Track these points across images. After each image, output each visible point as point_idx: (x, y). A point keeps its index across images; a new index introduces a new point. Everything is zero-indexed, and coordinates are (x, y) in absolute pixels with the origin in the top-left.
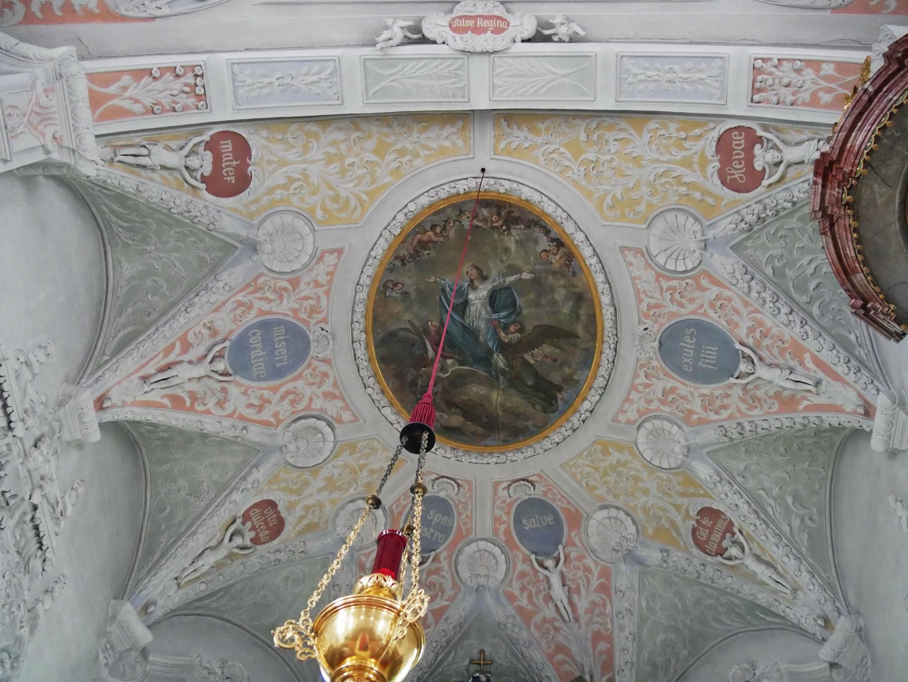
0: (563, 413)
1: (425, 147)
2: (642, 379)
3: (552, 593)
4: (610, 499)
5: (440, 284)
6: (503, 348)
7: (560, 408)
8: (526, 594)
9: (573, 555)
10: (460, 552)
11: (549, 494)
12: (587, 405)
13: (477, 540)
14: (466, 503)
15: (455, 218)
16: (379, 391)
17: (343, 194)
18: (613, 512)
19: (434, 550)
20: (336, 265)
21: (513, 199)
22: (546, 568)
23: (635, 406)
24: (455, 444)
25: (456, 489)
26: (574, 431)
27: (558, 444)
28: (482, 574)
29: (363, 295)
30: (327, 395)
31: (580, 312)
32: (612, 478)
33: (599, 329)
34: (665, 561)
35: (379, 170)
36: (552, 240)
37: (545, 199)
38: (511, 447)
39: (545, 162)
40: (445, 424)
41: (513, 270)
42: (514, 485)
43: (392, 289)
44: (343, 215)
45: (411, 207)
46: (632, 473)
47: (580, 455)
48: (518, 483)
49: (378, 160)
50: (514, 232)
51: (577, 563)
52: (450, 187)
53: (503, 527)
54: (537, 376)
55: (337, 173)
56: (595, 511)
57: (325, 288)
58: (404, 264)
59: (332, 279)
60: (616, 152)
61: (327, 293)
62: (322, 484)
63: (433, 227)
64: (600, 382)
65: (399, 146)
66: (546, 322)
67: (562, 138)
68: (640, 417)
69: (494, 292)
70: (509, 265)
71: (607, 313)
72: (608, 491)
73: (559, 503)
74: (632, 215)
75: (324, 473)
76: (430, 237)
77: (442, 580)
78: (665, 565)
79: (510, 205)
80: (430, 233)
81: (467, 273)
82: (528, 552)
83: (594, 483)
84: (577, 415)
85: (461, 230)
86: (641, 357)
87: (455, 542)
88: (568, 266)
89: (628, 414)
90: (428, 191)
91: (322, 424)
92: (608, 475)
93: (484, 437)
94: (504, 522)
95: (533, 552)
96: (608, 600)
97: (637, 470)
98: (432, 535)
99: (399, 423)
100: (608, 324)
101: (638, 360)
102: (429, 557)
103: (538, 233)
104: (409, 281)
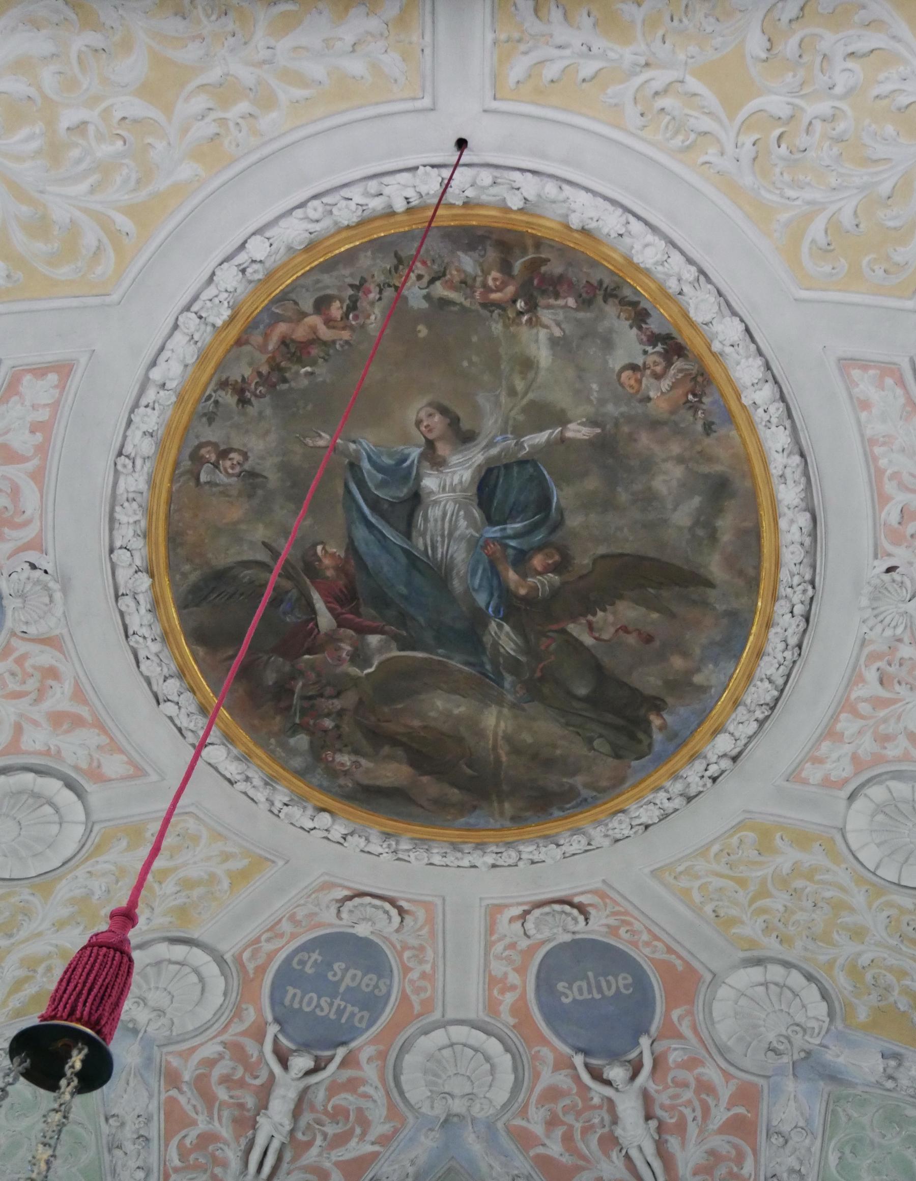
0: (662, 759)
1: (300, 80)
2: (871, 687)
3: (619, 1132)
4: (771, 946)
5: (345, 453)
6: (513, 608)
7: (657, 747)
8: (559, 1132)
9: (674, 1057)
10: (404, 1049)
11: (622, 931)
12: (724, 743)
13: (444, 1024)
14: (422, 949)
15: (380, 278)
16: (193, 708)
17: (60, 213)
18: (776, 972)
19: (344, 1044)
20: (55, 406)
21: (547, 225)
22: (608, 1083)
23: (847, 749)
24: (392, 825)
25: (396, 919)
26: (689, 799)
27: (647, 827)
28: (456, 1091)
29: (135, 482)
30: (58, 719)
31: (719, 523)
32: (778, 902)
33: (767, 565)
34: (891, 1077)
35: (160, 145)
36: (654, 339)
37: (636, 226)
38: (533, 830)
39: (640, 121)
40: (366, 781)
41: (543, 415)
42: (537, 912)
43: (216, 466)
44: (64, 272)
45: (258, 249)
46: (828, 894)
47: (703, 852)
48: (547, 909)
49: (153, 113)
50: (545, 316)
51: (683, 1075)
52: (366, 194)
53: (509, 998)
54: (598, 671)
55: (38, 153)
56: (734, 968)
57: (30, 466)
58: (243, 401)
59: (47, 439)
60: (849, 92)
61: (38, 476)
62: (65, 912)
63: (322, 304)
64: (762, 692)
65: (214, 75)
66: (628, 549)
67: (693, 49)
68: (856, 774)
69: (489, 471)
70: (532, 403)
71: (792, 527)
72: (767, 929)
73: (647, 951)
74: (880, 273)
75: (64, 889)
76: (314, 330)
77: (363, 1103)
78: (890, 1084)
79: (538, 243)
80: (315, 320)
81: (418, 423)
82: (566, 1050)
83: (734, 912)
84: (699, 765)
85: (397, 309)
86: (871, 635)
87: (395, 1027)
88: (694, 408)
89: (828, 766)
90: (302, 205)
91: (52, 786)
92: (768, 895)
93: (463, 809)
94: (513, 988)
95: (578, 1050)
96: (748, 1150)
97: (843, 889)
98: (340, 1012)
99: (247, 779)
100: (792, 556)
101: (863, 643)
102: (332, 1058)
103: (614, 319)
104: (260, 443)
